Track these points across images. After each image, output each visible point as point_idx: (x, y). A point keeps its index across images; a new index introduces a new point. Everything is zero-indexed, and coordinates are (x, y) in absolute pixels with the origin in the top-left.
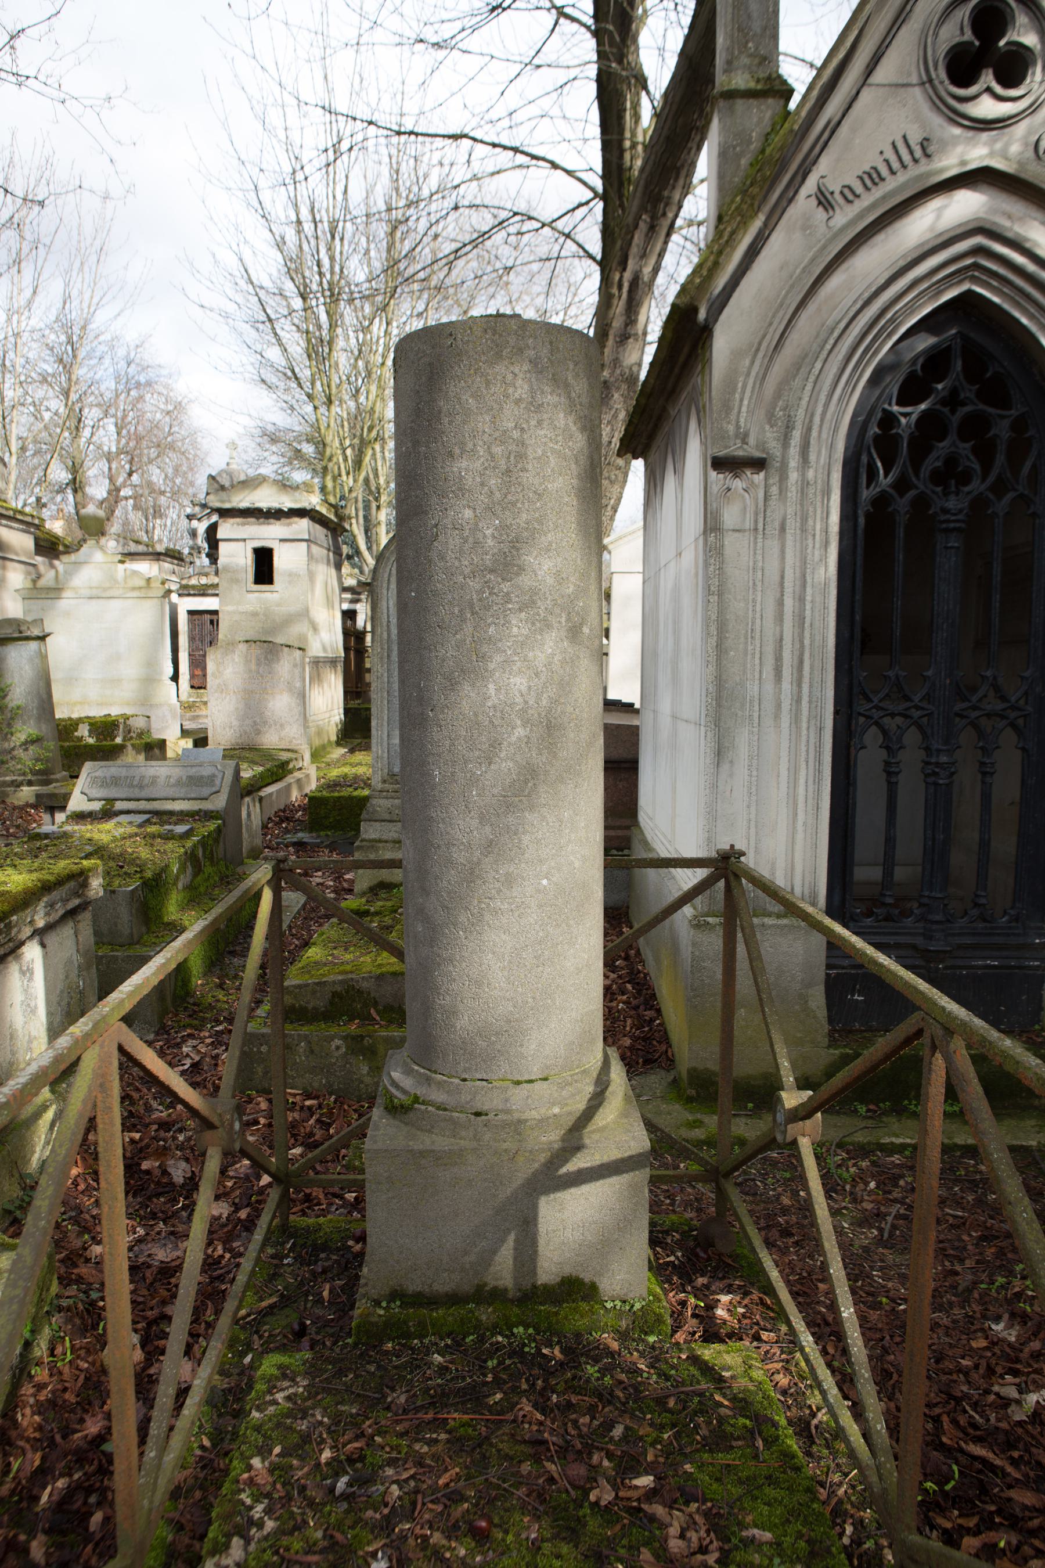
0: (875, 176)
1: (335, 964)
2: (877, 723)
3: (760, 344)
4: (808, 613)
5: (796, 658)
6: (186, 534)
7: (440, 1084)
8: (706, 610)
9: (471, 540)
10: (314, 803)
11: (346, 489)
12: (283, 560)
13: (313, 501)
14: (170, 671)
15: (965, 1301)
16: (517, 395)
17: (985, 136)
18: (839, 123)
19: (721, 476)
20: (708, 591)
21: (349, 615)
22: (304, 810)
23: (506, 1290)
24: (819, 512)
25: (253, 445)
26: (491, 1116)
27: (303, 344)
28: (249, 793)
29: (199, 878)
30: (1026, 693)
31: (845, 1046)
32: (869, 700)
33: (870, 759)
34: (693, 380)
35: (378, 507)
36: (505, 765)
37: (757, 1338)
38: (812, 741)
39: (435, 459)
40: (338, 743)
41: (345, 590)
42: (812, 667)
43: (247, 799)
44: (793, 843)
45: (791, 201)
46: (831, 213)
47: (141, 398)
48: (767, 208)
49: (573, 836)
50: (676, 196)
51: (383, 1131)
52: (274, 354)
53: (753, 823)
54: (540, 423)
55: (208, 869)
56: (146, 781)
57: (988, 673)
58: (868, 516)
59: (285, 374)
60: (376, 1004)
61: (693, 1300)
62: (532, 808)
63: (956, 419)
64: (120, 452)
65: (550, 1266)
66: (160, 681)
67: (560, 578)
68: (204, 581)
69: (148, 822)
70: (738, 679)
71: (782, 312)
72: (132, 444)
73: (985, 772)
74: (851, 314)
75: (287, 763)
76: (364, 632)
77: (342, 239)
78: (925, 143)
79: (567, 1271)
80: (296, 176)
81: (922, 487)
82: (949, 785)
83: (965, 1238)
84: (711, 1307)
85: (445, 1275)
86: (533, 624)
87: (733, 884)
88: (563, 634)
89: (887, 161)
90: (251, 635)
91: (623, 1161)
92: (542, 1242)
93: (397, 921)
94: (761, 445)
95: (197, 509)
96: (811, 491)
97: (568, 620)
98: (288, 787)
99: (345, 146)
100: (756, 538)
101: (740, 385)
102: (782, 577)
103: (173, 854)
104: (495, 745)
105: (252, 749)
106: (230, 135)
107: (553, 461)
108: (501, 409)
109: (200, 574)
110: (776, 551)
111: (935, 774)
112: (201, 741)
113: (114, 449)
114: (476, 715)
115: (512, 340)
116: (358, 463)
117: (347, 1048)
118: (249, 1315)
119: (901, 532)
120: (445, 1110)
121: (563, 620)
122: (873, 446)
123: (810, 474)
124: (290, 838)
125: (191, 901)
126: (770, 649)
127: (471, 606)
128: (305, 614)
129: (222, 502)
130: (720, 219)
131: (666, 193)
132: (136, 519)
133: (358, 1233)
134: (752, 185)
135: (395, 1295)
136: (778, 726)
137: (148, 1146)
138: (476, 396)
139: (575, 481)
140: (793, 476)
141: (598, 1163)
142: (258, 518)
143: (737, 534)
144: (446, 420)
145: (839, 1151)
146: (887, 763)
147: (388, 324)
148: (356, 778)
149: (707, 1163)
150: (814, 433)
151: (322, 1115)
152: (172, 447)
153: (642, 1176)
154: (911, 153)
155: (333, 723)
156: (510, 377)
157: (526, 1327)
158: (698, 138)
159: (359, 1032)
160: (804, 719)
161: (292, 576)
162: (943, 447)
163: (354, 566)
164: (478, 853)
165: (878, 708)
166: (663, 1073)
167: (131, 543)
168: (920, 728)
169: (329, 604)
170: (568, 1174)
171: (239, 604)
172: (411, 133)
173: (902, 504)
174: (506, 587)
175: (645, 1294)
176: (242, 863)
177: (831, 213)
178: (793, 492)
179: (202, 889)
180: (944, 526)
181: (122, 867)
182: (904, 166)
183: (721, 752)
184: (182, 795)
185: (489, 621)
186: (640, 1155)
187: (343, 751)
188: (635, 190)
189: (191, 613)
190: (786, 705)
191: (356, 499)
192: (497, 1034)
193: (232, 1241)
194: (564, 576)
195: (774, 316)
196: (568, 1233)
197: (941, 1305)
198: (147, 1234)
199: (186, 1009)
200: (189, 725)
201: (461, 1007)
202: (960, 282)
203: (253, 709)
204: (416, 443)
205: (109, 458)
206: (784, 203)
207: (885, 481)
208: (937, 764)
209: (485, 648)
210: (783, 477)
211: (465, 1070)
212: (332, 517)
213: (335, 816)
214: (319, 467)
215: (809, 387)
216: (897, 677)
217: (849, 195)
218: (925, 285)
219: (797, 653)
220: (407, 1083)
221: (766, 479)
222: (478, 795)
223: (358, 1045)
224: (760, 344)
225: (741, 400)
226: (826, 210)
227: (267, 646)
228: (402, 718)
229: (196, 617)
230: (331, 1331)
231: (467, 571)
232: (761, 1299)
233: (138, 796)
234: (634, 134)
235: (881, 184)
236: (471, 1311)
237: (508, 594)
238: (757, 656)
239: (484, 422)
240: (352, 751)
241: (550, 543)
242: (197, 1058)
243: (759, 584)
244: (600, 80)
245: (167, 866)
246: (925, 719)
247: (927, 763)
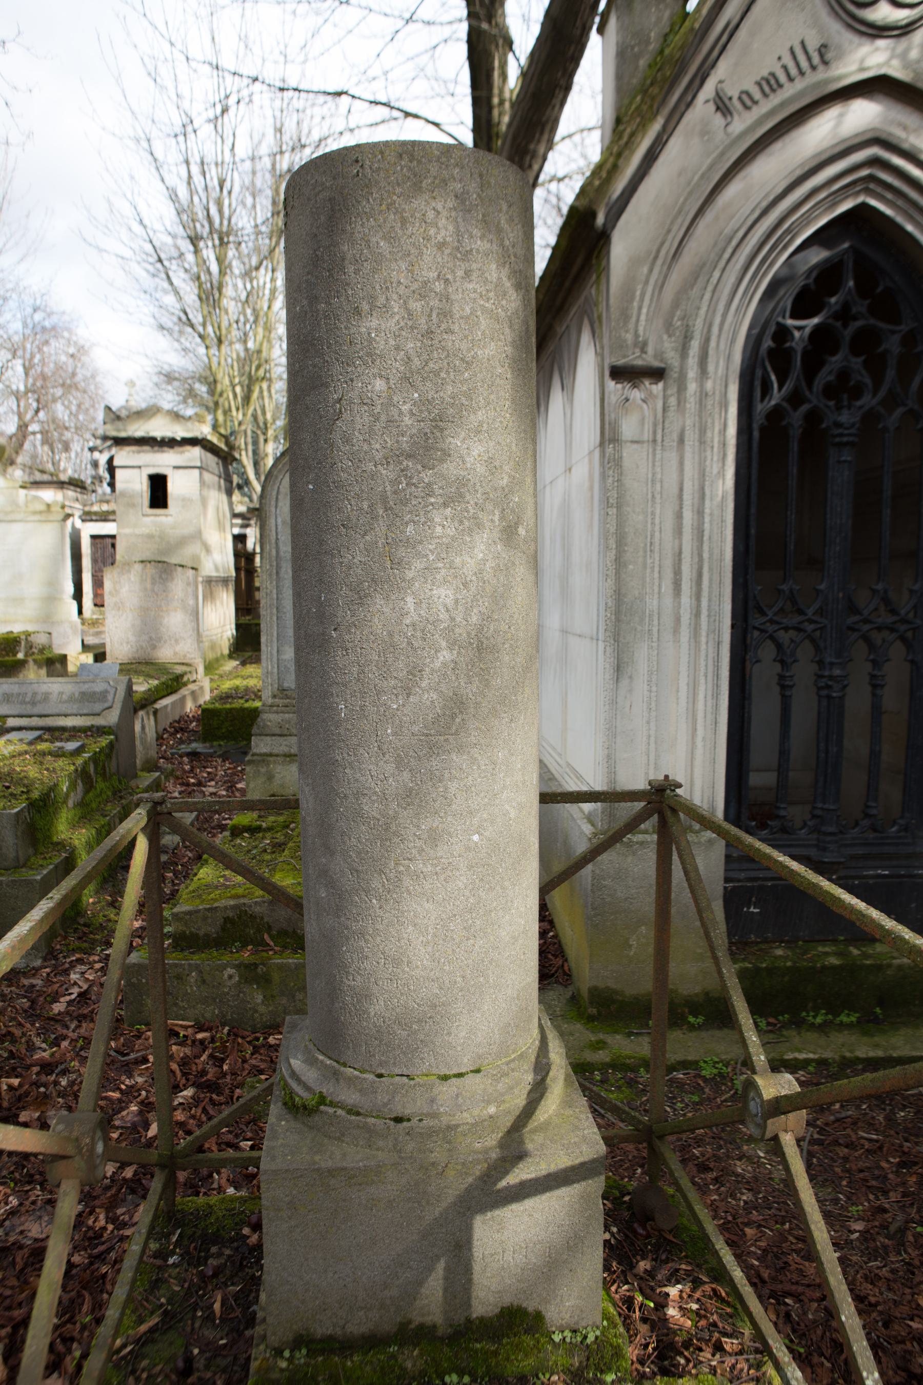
0: (773, 82)
1: (227, 887)
2: (771, 637)
3: (658, 251)
4: (707, 526)
5: (694, 571)
6: (89, 466)
7: (351, 1081)
8: (604, 522)
9: (383, 418)
10: (207, 715)
11: (236, 423)
12: (176, 486)
13: (204, 430)
14: (70, 588)
15: (901, 1245)
16: (440, 238)
17: (881, 43)
18: (737, 26)
19: (619, 386)
20: (606, 503)
21: (240, 539)
22: (198, 720)
23: (435, 1326)
24: (717, 424)
25: (151, 385)
26: (415, 1121)
27: (196, 291)
28: (143, 707)
29: (91, 794)
30: (915, 607)
31: (744, 960)
32: (764, 614)
33: (765, 671)
34: (585, 293)
35: (266, 441)
36: (428, 697)
37: (718, 1348)
38: (711, 656)
39: (337, 318)
40: (230, 657)
41: (235, 515)
42: (711, 580)
43: (141, 713)
44: (692, 759)
45: (689, 105)
46: (729, 119)
47: (47, 342)
48: (666, 111)
49: (508, 780)
50: (542, 150)
51: (283, 1144)
52: (170, 300)
53: (652, 739)
54: (468, 273)
55: (100, 785)
56: (39, 698)
57: (879, 587)
58: (762, 429)
59: (180, 319)
60: (269, 928)
61: (640, 1298)
62: (460, 749)
63: (848, 333)
64: (27, 391)
65: (490, 1289)
66: (60, 599)
67: (493, 467)
68: (105, 507)
69: (39, 739)
70: (636, 592)
71: (679, 220)
72: (39, 384)
73: (876, 685)
74: (749, 223)
75: (182, 676)
76: (253, 554)
77: (230, 193)
78: (823, 50)
79: (507, 1300)
80: (187, 129)
81: (815, 401)
82: (842, 698)
83: (884, 1164)
84: (661, 1305)
85: (361, 1313)
86: (461, 522)
87: (671, 819)
88: (496, 535)
89: (785, 68)
90: (146, 555)
91: (573, 1168)
92: (477, 1268)
93: (289, 838)
94: (659, 355)
95: (99, 442)
96: (710, 402)
97: (502, 518)
98: (183, 700)
99: (232, 101)
100: (654, 450)
101: (638, 293)
102: (681, 490)
103: (65, 768)
104: (415, 671)
105: (149, 663)
106: (123, 91)
107: (484, 323)
108: (421, 254)
109: (101, 501)
110: (674, 463)
111: (828, 687)
112: (100, 657)
113: (22, 388)
114: (391, 635)
115: (434, 169)
116: (247, 399)
117: (240, 976)
118: (124, 1346)
119: (795, 446)
120: (358, 1114)
121: (496, 518)
122: (769, 356)
123: (709, 385)
124: (184, 748)
125: (83, 817)
126: (668, 563)
127: (384, 499)
128: (198, 535)
129: (119, 430)
130: (618, 121)
131: (532, 147)
132: (43, 451)
133: (254, 1219)
134: (652, 84)
135: (298, 1342)
136: (677, 641)
137: (27, 1094)
138: (390, 238)
139: (509, 349)
140: (692, 387)
141: (544, 1173)
142: (152, 447)
143: (635, 446)
144: (351, 269)
145: (744, 1070)
146: (781, 677)
147: (273, 271)
148: (247, 690)
149: (640, 1122)
150: (713, 344)
151: (214, 1049)
152: (75, 386)
153: (596, 1185)
154: (809, 59)
155: (225, 637)
156: (431, 215)
157: (461, 1375)
158: (561, 96)
159: (253, 959)
160: (704, 633)
161: (185, 501)
162: (836, 361)
163: (244, 495)
164: (394, 805)
165: (771, 621)
166: (561, 988)
167: (37, 473)
168: (813, 641)
169: (221, 527)
170: (508, 1188)
171: (136, 527)
172: (295, 90)
173: (796, 418)
174: (427, 476)
175: (598, 1318)
176: (135, 776)
177: (729, 119)
178: (691, 404)
179: (94, 805)
180: (837, 440)
181: (8, 788)
182: (802, 73)
183: (620, 668)
184: (75, 711)
185: (407, 518)
186: (594, 1161)
187: (235, 663)
188: (503, 144)
189: (93, 537)
190: (686, 618)
191: (245, 432)
192: (420, 1021)
193: (116, 1207)
194: (497, 464)
195: (672, 223)
196: (509, 1257)
197: (876, 1250)
198: (21, 1204)
199: (76, 930)
200: (90, 640)
201: (375, 990)
202: (858, 193)
203: (149, 626)
204: (314, 300)
205: (17, 395)
206: (683, 107)
207: (776, 396)
208: (831, 678)
209: (401, 552)
210: (682, 388)
211: (381, 1064)
212: (223, 446)
213: (228, 728)
214: (211, 405)
215: (707, 296)
216: (791, 591)
217: (747, 101)
218: (822, 195)
219: (696, 567)
220: (310, 1075)
221: (665, 389)
222: (395, 734)
223: (251, 974)
224: (658, 251)
225: (640, 308)
226: (724, 115)
227: (162, 566)
228: (297, 638)
229: (98, 541)
230: (222, 1362)
231: (378, 456)
232: (714, 1290)
233: (29, 712)
234: (501, 91)
235: (779, 92)
236: (393, 1357)
237: (429, 485)
238: (656, 569)
239: (399, 271)
240: (243, 663)
241: (481, 424)
242: (85, 987)
243: (658, 496)
244: (470, 42)
245: (56, 785)
246: (818, 633)
247: (822, 676)
